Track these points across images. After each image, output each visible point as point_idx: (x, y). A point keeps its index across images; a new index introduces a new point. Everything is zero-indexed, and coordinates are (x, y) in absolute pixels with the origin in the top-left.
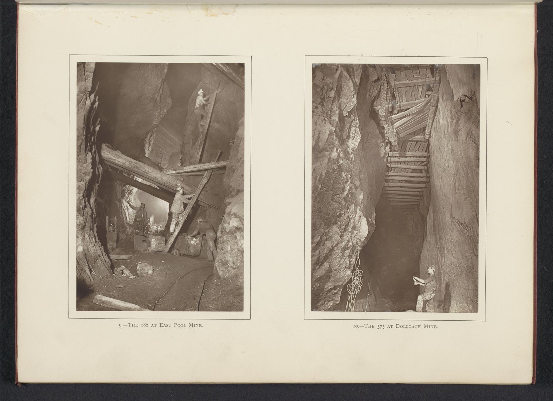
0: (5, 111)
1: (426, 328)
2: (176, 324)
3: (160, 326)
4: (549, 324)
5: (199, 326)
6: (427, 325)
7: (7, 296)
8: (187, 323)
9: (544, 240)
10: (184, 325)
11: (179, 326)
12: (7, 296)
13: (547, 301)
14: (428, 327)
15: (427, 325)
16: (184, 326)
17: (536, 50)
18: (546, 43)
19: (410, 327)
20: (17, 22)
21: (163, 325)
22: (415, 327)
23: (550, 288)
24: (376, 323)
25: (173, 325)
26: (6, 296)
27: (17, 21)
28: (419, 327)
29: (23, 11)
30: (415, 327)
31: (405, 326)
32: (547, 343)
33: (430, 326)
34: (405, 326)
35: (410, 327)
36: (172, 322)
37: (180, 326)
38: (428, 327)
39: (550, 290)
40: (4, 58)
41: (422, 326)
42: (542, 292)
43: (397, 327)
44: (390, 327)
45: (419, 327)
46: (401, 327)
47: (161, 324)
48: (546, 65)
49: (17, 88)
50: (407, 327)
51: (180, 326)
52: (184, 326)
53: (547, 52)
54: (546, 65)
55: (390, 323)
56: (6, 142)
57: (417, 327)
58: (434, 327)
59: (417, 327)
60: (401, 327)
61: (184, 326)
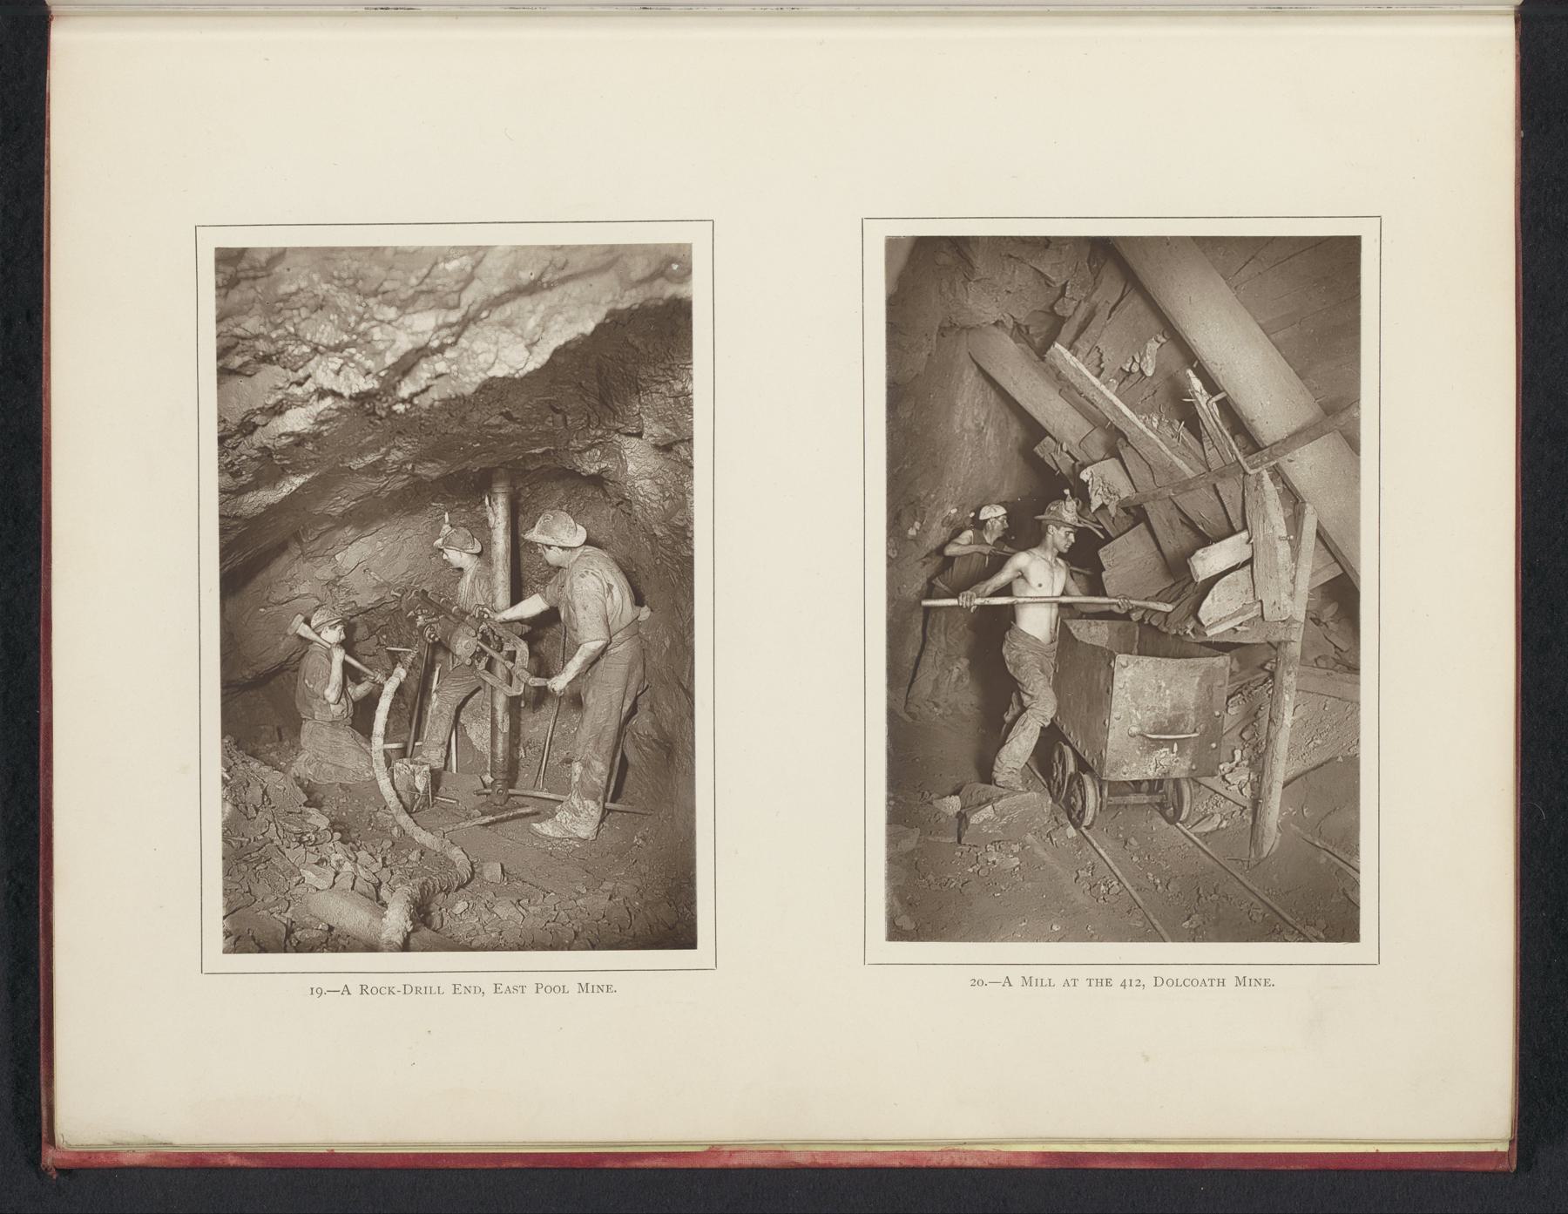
0: (9, 358)
1: (1242, 987)
2: (540, 986)
3: (496, 992)
4: (1549, 966)
5: (605, 989)
6: (587, 984)
7: (13, 884)
8: (486, 982)
9: (1535, 727)
10: (562, 988)
11: (548, 989)
12: (13, 884)
13: (1543, 901)
14: (1247, 983)
15: (587, 984)
16: (1175, 984)
17: (1520, 233)
18: (1543, 167)
19: (1195, 983)
20: (46, 143)
21: (503, 988)
22: (1208, 983)
23: (1552, 863)
24: (1117, 974)
25: (531, 989)
26: (10, 884)
27: (46, 139)
28: (1222, 982)
29: (65, 40)
30: (1208, 983)
31: (1180, 982)
32: (1543, 1022)
33: (1253, 981)
34: (1180, 982)
35: (1195, 983)
36: (1229, 974)
37: (553, 989)
38: (1247, 983)
39: (1552, 871)
40: (6, 206)
41: (1231, 982)
42: (1529, 874)
43: (1156, 985)
44: (1071, 983)
45: (1222, 982)
46: (1170, 983)
47: (498, 986)
48: (1541, 229)
49: (49, 149)
50: (1187, 983)
51: (553, 989)
52: (563, 989)
53: (1546, 193)
54: (1541, 229)
55: (1070, 972)
56: (11, 446)
57: (1215, 983)
58: (1263, 982)
59: (1215, 983)
60: (1170, 983)
61: (563, 989)
